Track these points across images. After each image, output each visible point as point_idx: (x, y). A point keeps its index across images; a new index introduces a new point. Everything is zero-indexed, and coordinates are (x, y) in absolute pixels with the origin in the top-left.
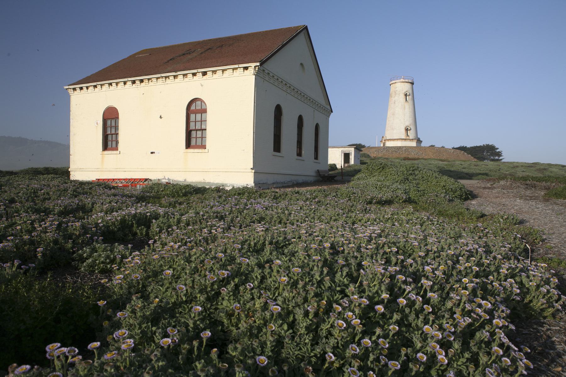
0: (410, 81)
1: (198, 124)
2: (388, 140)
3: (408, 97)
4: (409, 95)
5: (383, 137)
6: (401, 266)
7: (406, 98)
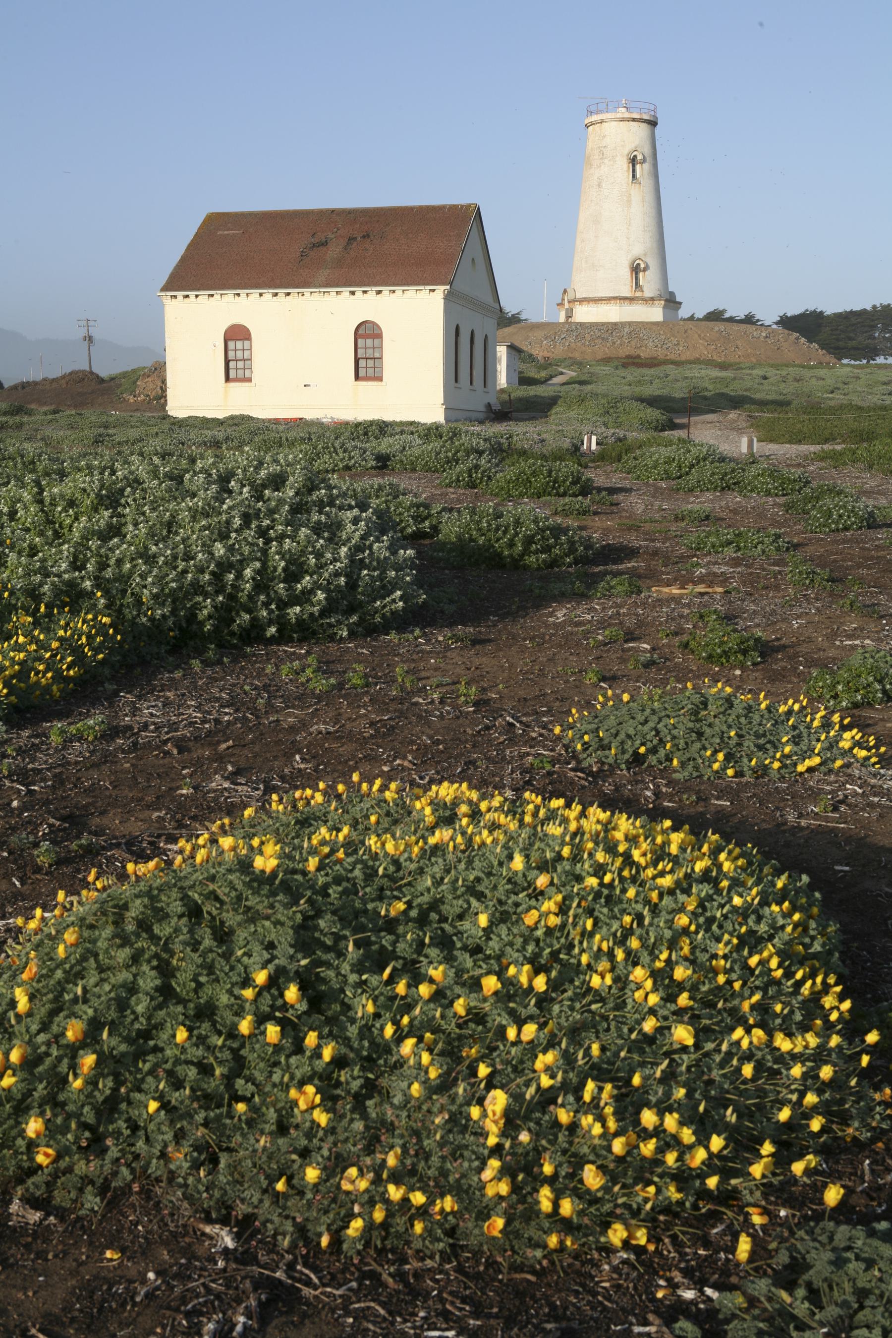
0: (646, 117)
1: (370, 352)
2: (582, 301)
3: (638, 167)
4: (644, 161)
5: (565, 291)
6: (695, 1283)
7: (634, 171)
